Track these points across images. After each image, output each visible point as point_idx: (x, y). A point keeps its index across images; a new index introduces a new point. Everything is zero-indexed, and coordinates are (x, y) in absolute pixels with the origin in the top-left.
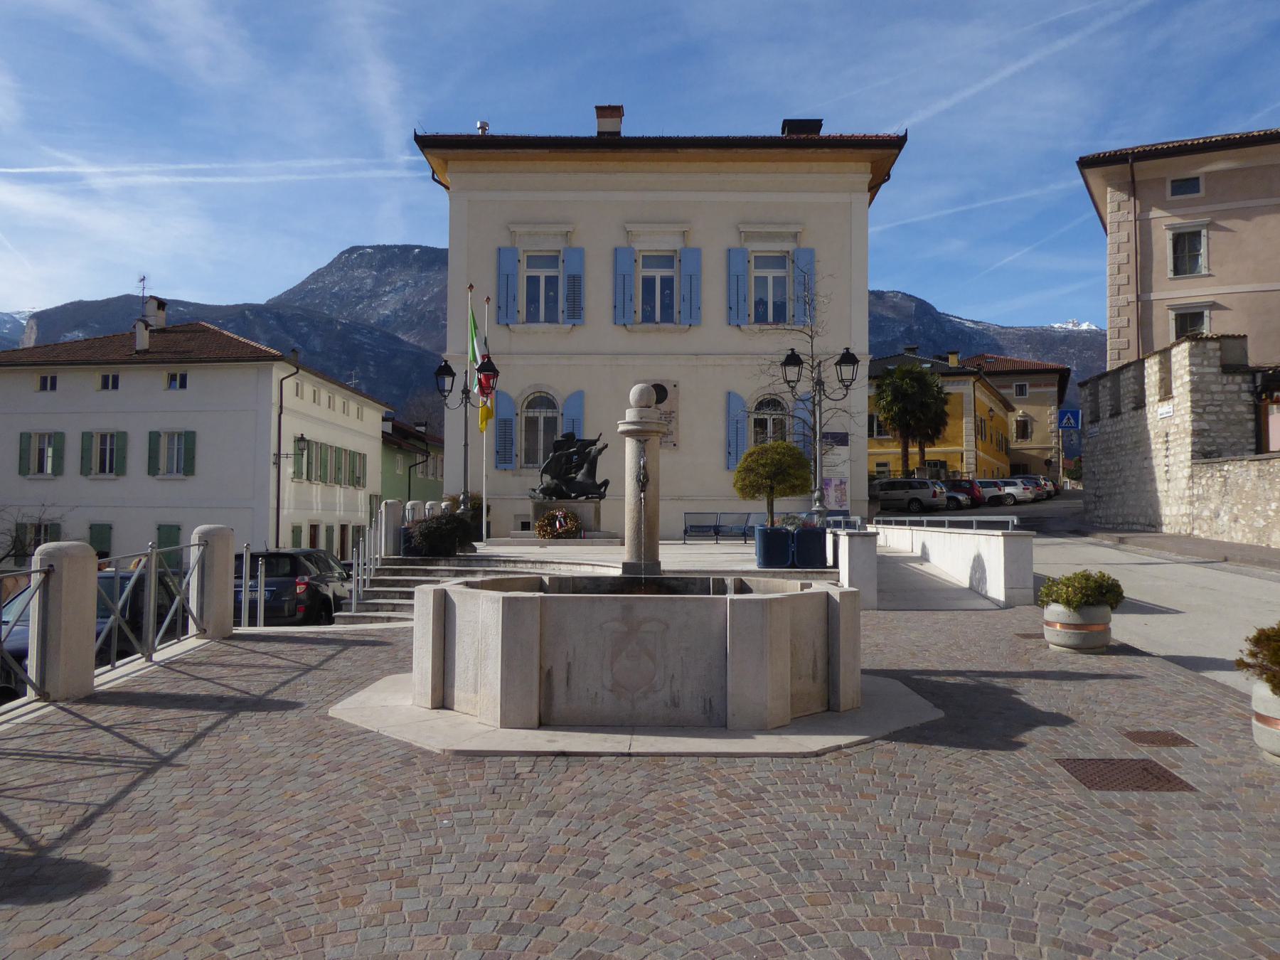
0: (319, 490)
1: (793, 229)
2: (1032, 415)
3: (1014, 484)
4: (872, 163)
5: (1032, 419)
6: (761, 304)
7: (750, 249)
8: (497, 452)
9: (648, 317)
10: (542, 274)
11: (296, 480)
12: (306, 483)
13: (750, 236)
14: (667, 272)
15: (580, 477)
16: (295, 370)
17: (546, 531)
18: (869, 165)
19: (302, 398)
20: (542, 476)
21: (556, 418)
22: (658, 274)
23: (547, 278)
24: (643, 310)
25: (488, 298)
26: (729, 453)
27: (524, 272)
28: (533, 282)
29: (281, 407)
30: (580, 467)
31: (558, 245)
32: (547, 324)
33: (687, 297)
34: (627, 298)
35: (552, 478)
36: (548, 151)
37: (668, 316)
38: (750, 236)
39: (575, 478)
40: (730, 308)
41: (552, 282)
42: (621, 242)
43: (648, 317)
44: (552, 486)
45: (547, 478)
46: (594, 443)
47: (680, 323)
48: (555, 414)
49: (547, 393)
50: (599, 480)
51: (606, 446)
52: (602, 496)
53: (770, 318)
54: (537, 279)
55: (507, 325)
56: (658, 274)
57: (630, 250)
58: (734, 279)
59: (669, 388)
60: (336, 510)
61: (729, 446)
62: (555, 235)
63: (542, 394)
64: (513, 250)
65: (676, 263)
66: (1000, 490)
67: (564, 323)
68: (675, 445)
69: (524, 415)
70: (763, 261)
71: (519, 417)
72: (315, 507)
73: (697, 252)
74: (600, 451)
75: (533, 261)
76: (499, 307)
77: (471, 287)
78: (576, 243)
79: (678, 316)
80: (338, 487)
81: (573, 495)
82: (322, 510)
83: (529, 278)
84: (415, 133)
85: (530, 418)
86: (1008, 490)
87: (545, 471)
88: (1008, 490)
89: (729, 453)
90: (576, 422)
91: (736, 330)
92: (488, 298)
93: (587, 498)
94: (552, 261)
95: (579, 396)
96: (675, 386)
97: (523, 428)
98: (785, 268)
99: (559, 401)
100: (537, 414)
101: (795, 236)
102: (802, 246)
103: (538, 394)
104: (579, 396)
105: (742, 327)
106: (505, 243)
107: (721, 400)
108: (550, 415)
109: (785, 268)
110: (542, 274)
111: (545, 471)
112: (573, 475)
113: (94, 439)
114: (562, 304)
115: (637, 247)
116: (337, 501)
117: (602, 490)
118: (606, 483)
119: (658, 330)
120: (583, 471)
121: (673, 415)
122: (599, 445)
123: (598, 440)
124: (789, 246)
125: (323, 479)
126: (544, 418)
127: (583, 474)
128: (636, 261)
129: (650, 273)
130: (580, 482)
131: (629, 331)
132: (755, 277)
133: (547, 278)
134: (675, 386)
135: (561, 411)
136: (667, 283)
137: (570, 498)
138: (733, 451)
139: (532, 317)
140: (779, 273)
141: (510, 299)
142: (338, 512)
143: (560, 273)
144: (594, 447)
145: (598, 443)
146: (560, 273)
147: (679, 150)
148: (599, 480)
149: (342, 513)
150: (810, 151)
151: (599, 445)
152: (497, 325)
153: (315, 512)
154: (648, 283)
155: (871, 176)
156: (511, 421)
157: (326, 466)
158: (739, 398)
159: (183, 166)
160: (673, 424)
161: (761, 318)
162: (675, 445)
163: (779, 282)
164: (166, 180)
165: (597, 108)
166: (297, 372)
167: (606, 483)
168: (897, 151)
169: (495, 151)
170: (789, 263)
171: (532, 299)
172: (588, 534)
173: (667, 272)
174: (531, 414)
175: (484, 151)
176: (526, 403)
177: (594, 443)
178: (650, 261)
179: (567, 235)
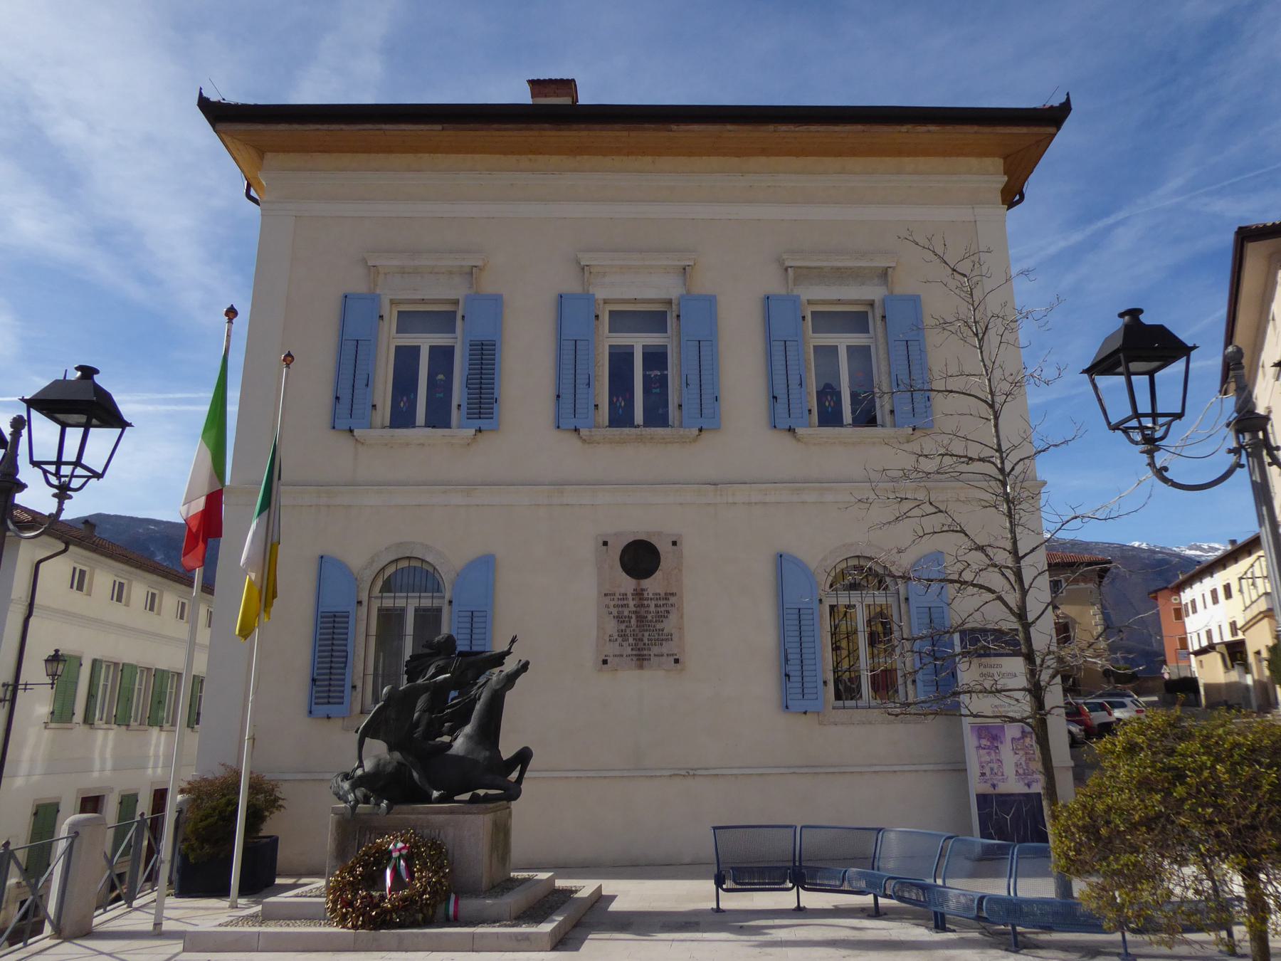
0: (110, 744)
1: (881, 263)
2: (1072, 616)
3: (1123, 705)
4: (1005, 158)
5: (1075, 622)
6: (828, 393)
7: (804, 298)
8: (314, 680)
9: (620, 418)
10: (425, 342)
11: (53, 725)
12: (85, 728)
13: (804, 275)
14: (654, 339)
15: (459, 745)
16: (62, 546)
17: (349, 904)
18: (999, 163)
19: (127, 605)
20: (361, 744)
21: (439, 610)
22: (639, 342)
23: (433, 349)
24: (611, 402)
25: (289, 355)
26: (787, 675)
27: (390, 339)
28: (406, 357)
29: (31, 606)
30: (461, 718)
31: (457, 290)
32: (430, 429)
33: (694, 380)
34: (582, 380)
35: (391, 749)
36: (439, 127)
37: (657, 416)
38: (804, 275)
39: (449, 745)
40: (775, 398)
41: (442, 357)
42: (572, 286)
43: (620, 418)
44: (390, 768)
45: (377, 750)
46: (499, 659)
47: (681, 426)
48: (436, 603)
49: (423, 561)
50: (507, 749)
51: (524, 667)
52: (512, 793)
53: (847, 416)
54: (415, 350)
55: (351, 431)
56: (639, 342)
57: (588, 298)
58: (778, 347)
59: (663, 547)
60: (145, 768)
61: (787, 660)
62: (451, 273)
63: (413, 563)
64: (373, 298)
65: (671, 321)
66: (1110, 714)
67: (460, 427)
68: (677, 661)
69: (376, 604)
70: (827, 320)
71: (364, 609)
72: (97, 765)
73: (710, 302)
74: (511, 679)
75: (408, 321)
76: (337, 398)
77: (289, 358)
78: (489, 285)
79: (677, 413)
80: (155, 731)
81: (436, 794)
82: (114, 769)
83: (399, 349)
84: (201, 94)
85: (388, 609)
86: (1117, 713)
87: (370, 731)
88: (1117, 713)
89: (787, 675)
90: (477, 618)
91: (787, 439)
92: (289, 355)
93: (475, 800)
94: (444, 320)
95: (486, 564)
96: (674, 543)
97: (373, 630)
98: (868, 332)
99: (447, 577)
100: (400, 603)
101: (884, 275)
102: (899, 290)
103: (404, 564)
104: (486, 564)
105: (800, 431)
106: (358, 285)
107: (763, 573)
108: (426, 603)
109: (868, 332)
110: (425, 342)
111: (370, 731)
112: (446, 739)
113: (83, 668)
114: (458, 393)
115: (600, 294)
116: (152, 753)
117: (514, 776)
118: (523, 757)
119: (640, 440)
120: (468, 729)
121: (672, 600)
122: (510, 665)
123: (508, 653)
124: (873, 292)
125: (122, 720)
126: (416, 610)
127: (469, 737)
128: (597, 317)
129: (623, 339)
130: (457, 758)
131: (584, 441)
132: (814, 346)
133: (433, 349)
134: (674, 543)
135: (448, 596)
136: (656, 359)
137: (428, 800)
138: (794, 669)
139: (402, 418)
140: (858, 339)
141: (360, 383)
142: (150, 771)
143: (458, 340)
144: (496, 670)
145: (507, 659)
146: (458, 340)
147: (674, 127)
148: (507, 749)
149: (159, 771)
150: (904, 128)
151: (510, 665)
152: (333, 431)
153: (96, 774)
154: (621, 360)
155: (1006, 178)
156: (346, 615)
157: (129, 700)
158: (797, 562)
159: (171, 396)
160: (673, 617)
161: (830, 417)
162: (677, 661)
163: (860, 355)
164: (150, 408)
165: (531, 82)
166: (65, 550)
167: (523, 757)
168: (1051, 130)
169: (343, 127)
170: (875, 324)
171: (404, 384)
172: (470, 905)
173: (654, 339)
174: (388, 603)
175: (325, 127)
176: (379, 583)
177: (499, 659)
178: (622, 319)
179: (471, 273)
